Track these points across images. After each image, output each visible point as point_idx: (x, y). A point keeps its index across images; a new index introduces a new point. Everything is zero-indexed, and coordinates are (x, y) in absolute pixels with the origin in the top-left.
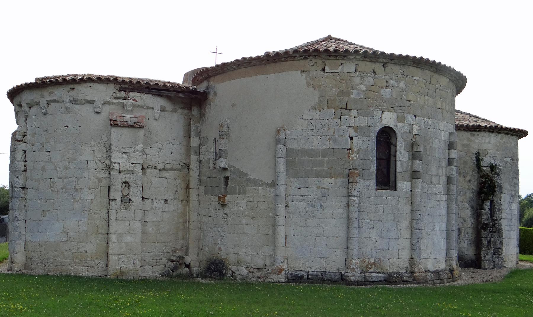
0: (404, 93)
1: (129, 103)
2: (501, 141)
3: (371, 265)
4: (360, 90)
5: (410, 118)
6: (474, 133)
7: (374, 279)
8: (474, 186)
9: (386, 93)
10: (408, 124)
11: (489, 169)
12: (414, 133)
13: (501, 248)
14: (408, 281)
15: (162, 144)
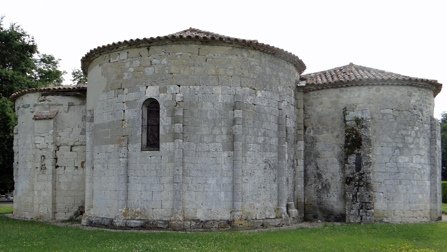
0: (167, 67)
1: (46, 103)
2: (376, 93)
3: (138, 213)
4: (130, 72)
5: (172, 88)
6: (342, 89)
7: (133, 225)
8: (342, 141)
9: (149, 71)
10: (171, 93)
11: (354, 123)
12: (177, 101)
13: (370, 203)
14: (163, 228)
15: (72, 128)
